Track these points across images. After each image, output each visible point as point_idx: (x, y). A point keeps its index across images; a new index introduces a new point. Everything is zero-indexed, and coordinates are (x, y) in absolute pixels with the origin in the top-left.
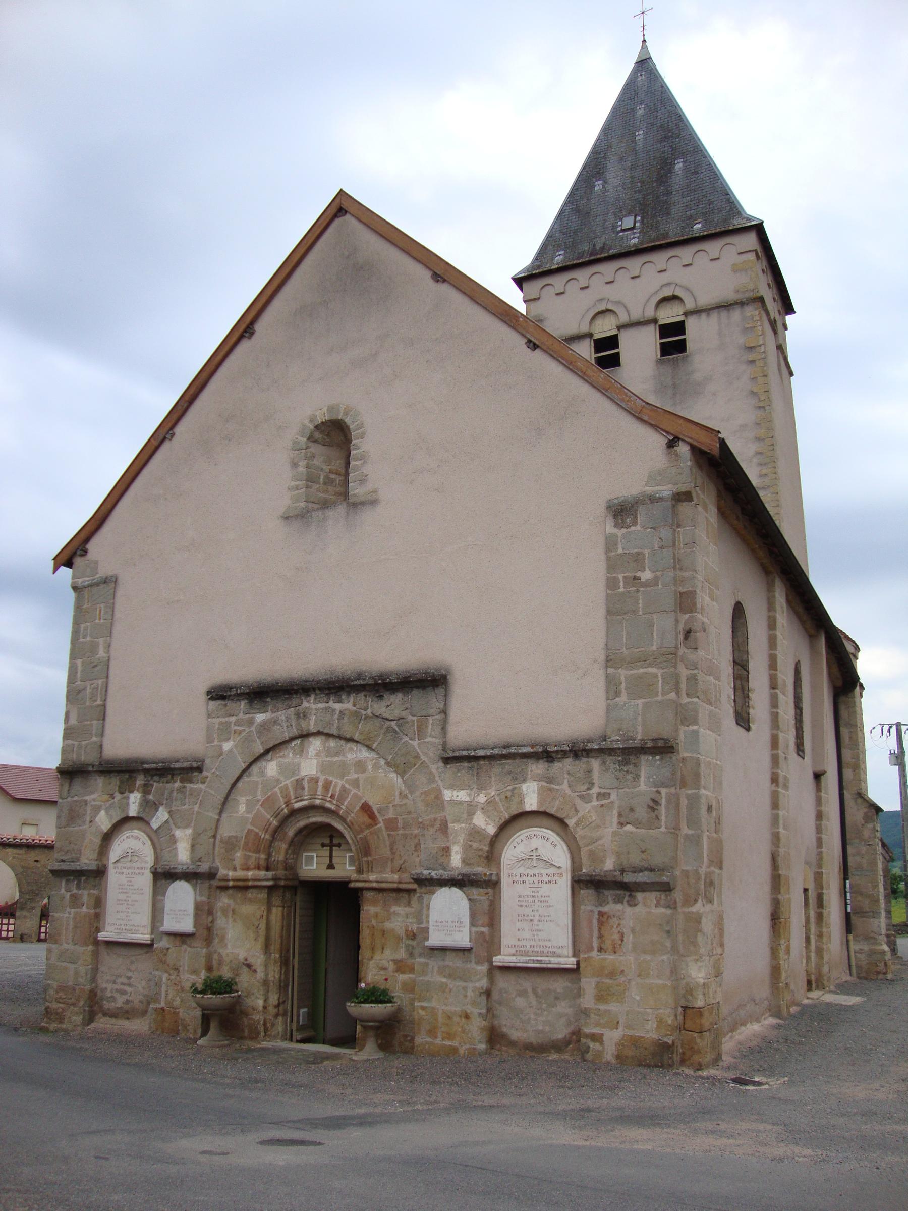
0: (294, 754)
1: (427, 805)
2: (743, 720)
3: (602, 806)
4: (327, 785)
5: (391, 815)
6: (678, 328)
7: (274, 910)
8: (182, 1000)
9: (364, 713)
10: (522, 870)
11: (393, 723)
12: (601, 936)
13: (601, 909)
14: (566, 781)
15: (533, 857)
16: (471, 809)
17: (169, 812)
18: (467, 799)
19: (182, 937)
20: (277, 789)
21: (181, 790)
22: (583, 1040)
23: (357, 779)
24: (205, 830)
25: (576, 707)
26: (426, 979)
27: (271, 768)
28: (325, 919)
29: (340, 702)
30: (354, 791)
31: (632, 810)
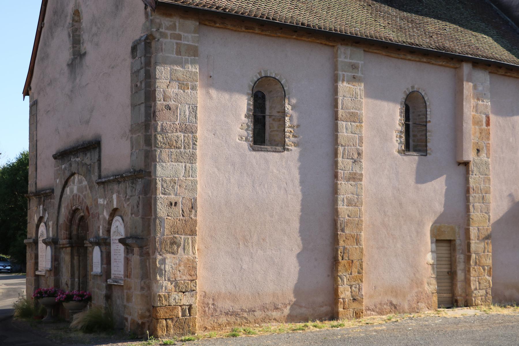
4: (79, 196)
27: (68, 190)
29: (77, 157)
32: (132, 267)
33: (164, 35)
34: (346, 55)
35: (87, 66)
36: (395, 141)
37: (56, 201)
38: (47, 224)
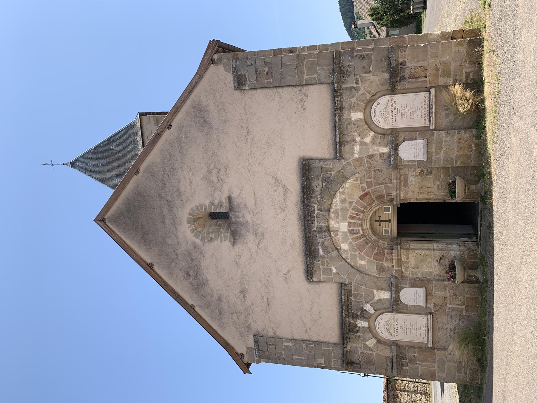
0: (337, 235)
1: (360, 165)
3: (362, 81)
4: (352, 218)
5: (365, 185)
7: (412, 247)
8: (461, 295)
9: (319, 199)
10: (390, 118)
11: (324, 184)
12: (420, 77)
13: (407, 78)
14: (351, 100)
15: (383, 114)
16: (362, 144)
17: (366, 303)
18: (358, 146)
19: (428, 295)
20: (354, 244)
22: (469, 82)
23: (349, 202)
24: (374, 282)
25: (319, 97)
26: (442, 161)
28: (416, 219)
29: (314, 211)
30: (354, 204)
31: (364, 67)
32: (417, 65)
35: (240, 194)
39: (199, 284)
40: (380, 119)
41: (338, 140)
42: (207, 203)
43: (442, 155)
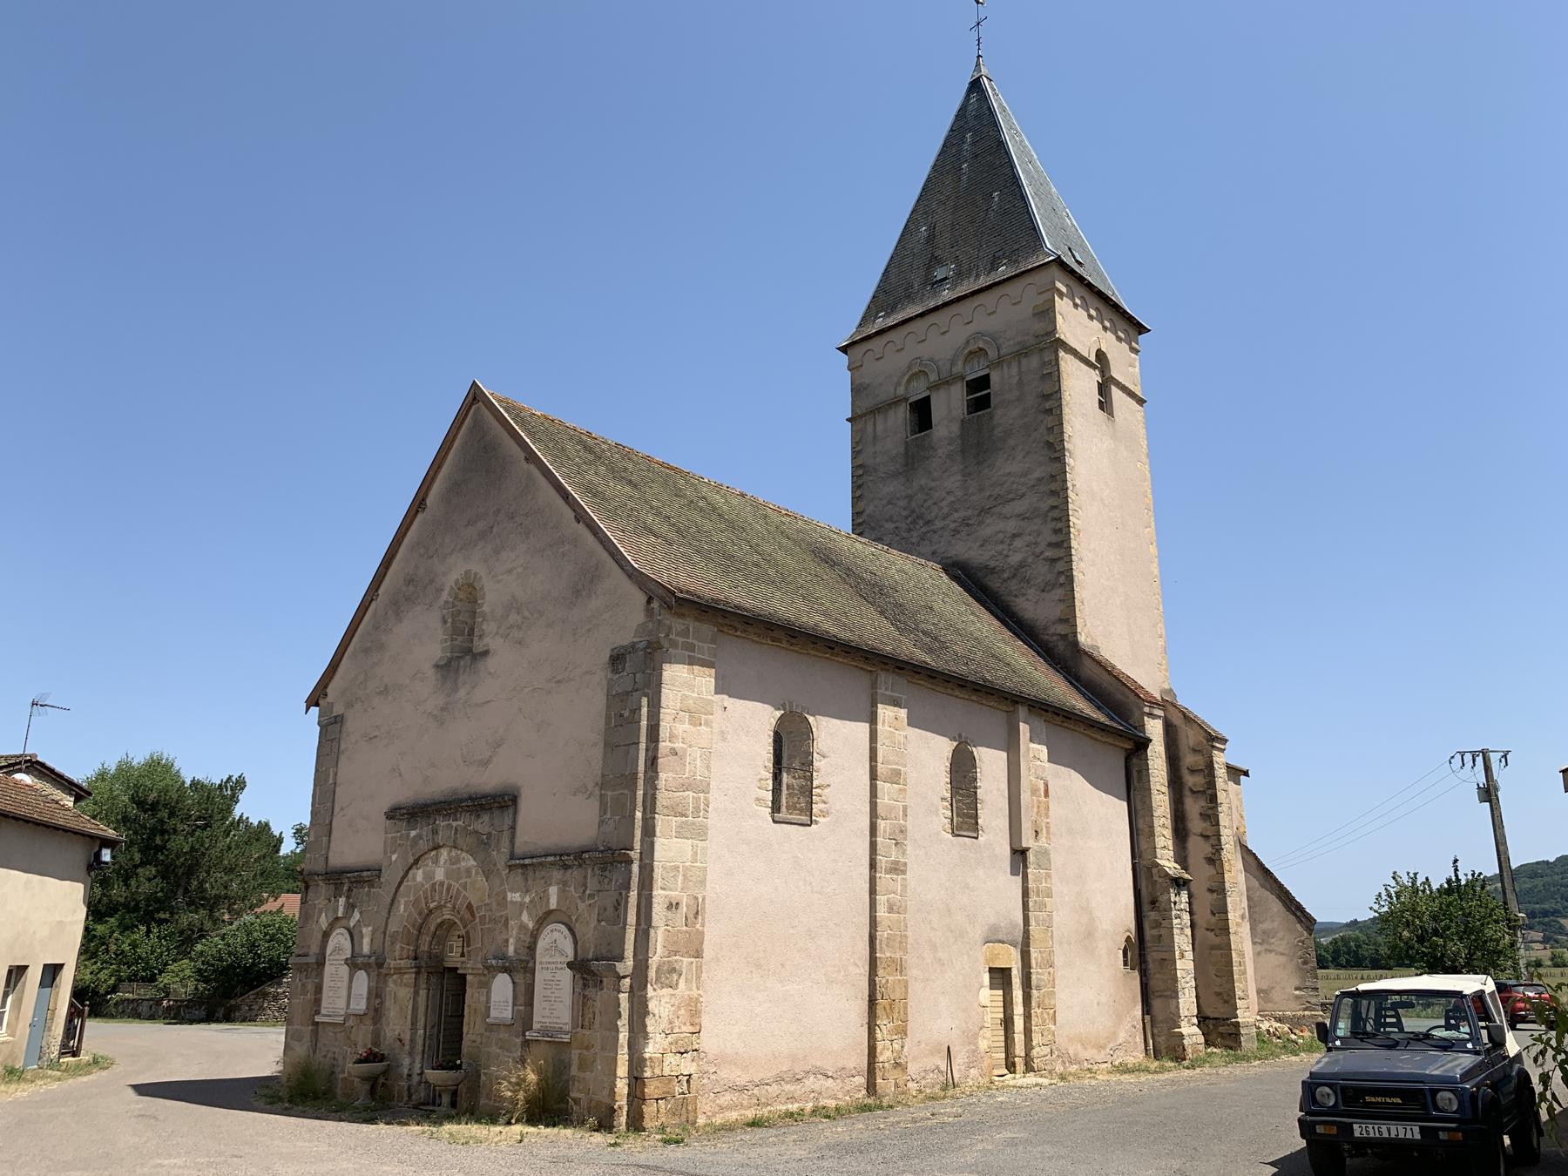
2: (966, 819)
6: (984, 382)
21: (368, 894)
27: (419, 875)
33: (674, 644)
34: (886, 680)
36: (942, 816)
37: (385, 894)
38: (355, 933)
39: (398, 607)
40: (548, 940)
41: (527, 861)
42: (485, 608)
43: (495, 1050)
